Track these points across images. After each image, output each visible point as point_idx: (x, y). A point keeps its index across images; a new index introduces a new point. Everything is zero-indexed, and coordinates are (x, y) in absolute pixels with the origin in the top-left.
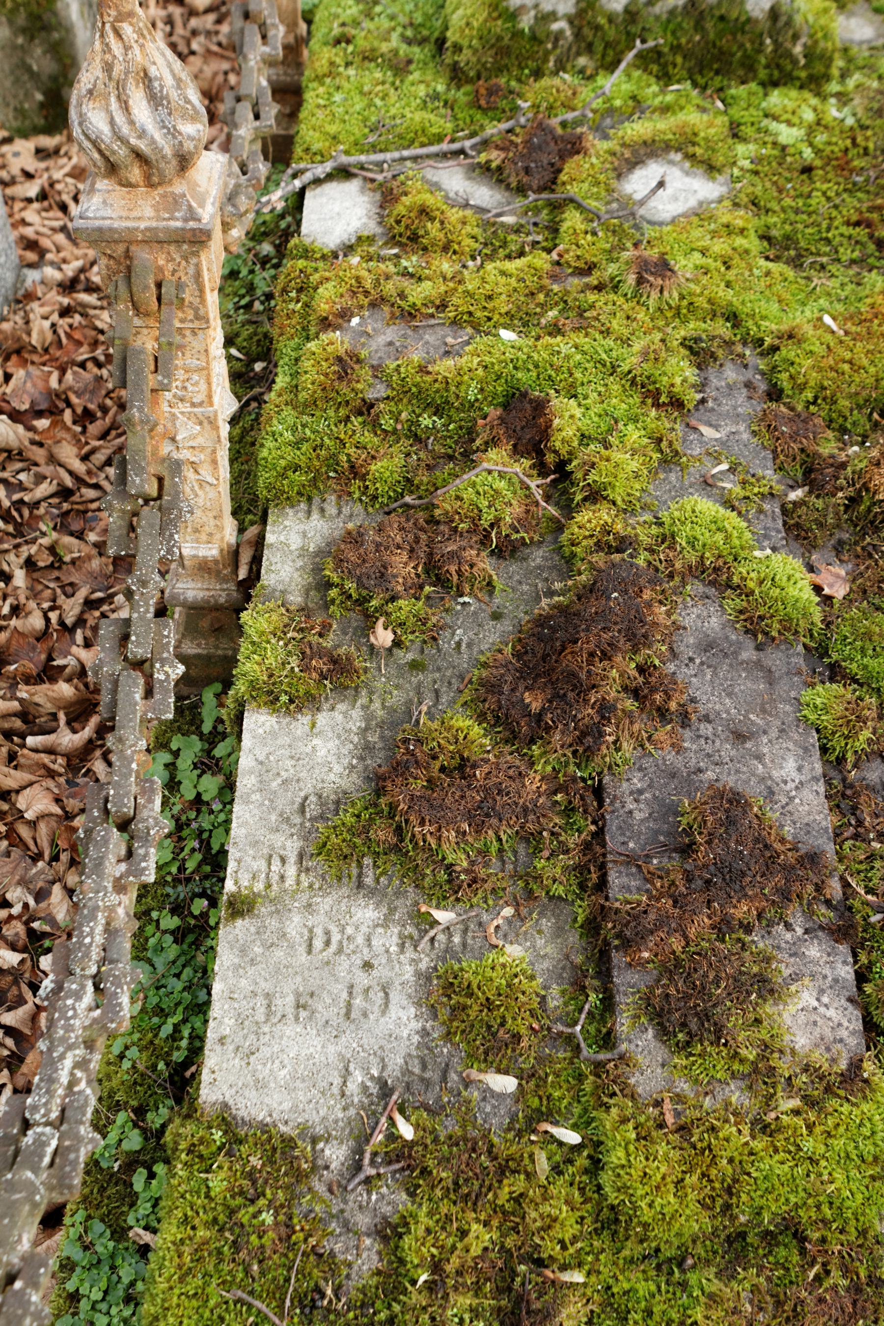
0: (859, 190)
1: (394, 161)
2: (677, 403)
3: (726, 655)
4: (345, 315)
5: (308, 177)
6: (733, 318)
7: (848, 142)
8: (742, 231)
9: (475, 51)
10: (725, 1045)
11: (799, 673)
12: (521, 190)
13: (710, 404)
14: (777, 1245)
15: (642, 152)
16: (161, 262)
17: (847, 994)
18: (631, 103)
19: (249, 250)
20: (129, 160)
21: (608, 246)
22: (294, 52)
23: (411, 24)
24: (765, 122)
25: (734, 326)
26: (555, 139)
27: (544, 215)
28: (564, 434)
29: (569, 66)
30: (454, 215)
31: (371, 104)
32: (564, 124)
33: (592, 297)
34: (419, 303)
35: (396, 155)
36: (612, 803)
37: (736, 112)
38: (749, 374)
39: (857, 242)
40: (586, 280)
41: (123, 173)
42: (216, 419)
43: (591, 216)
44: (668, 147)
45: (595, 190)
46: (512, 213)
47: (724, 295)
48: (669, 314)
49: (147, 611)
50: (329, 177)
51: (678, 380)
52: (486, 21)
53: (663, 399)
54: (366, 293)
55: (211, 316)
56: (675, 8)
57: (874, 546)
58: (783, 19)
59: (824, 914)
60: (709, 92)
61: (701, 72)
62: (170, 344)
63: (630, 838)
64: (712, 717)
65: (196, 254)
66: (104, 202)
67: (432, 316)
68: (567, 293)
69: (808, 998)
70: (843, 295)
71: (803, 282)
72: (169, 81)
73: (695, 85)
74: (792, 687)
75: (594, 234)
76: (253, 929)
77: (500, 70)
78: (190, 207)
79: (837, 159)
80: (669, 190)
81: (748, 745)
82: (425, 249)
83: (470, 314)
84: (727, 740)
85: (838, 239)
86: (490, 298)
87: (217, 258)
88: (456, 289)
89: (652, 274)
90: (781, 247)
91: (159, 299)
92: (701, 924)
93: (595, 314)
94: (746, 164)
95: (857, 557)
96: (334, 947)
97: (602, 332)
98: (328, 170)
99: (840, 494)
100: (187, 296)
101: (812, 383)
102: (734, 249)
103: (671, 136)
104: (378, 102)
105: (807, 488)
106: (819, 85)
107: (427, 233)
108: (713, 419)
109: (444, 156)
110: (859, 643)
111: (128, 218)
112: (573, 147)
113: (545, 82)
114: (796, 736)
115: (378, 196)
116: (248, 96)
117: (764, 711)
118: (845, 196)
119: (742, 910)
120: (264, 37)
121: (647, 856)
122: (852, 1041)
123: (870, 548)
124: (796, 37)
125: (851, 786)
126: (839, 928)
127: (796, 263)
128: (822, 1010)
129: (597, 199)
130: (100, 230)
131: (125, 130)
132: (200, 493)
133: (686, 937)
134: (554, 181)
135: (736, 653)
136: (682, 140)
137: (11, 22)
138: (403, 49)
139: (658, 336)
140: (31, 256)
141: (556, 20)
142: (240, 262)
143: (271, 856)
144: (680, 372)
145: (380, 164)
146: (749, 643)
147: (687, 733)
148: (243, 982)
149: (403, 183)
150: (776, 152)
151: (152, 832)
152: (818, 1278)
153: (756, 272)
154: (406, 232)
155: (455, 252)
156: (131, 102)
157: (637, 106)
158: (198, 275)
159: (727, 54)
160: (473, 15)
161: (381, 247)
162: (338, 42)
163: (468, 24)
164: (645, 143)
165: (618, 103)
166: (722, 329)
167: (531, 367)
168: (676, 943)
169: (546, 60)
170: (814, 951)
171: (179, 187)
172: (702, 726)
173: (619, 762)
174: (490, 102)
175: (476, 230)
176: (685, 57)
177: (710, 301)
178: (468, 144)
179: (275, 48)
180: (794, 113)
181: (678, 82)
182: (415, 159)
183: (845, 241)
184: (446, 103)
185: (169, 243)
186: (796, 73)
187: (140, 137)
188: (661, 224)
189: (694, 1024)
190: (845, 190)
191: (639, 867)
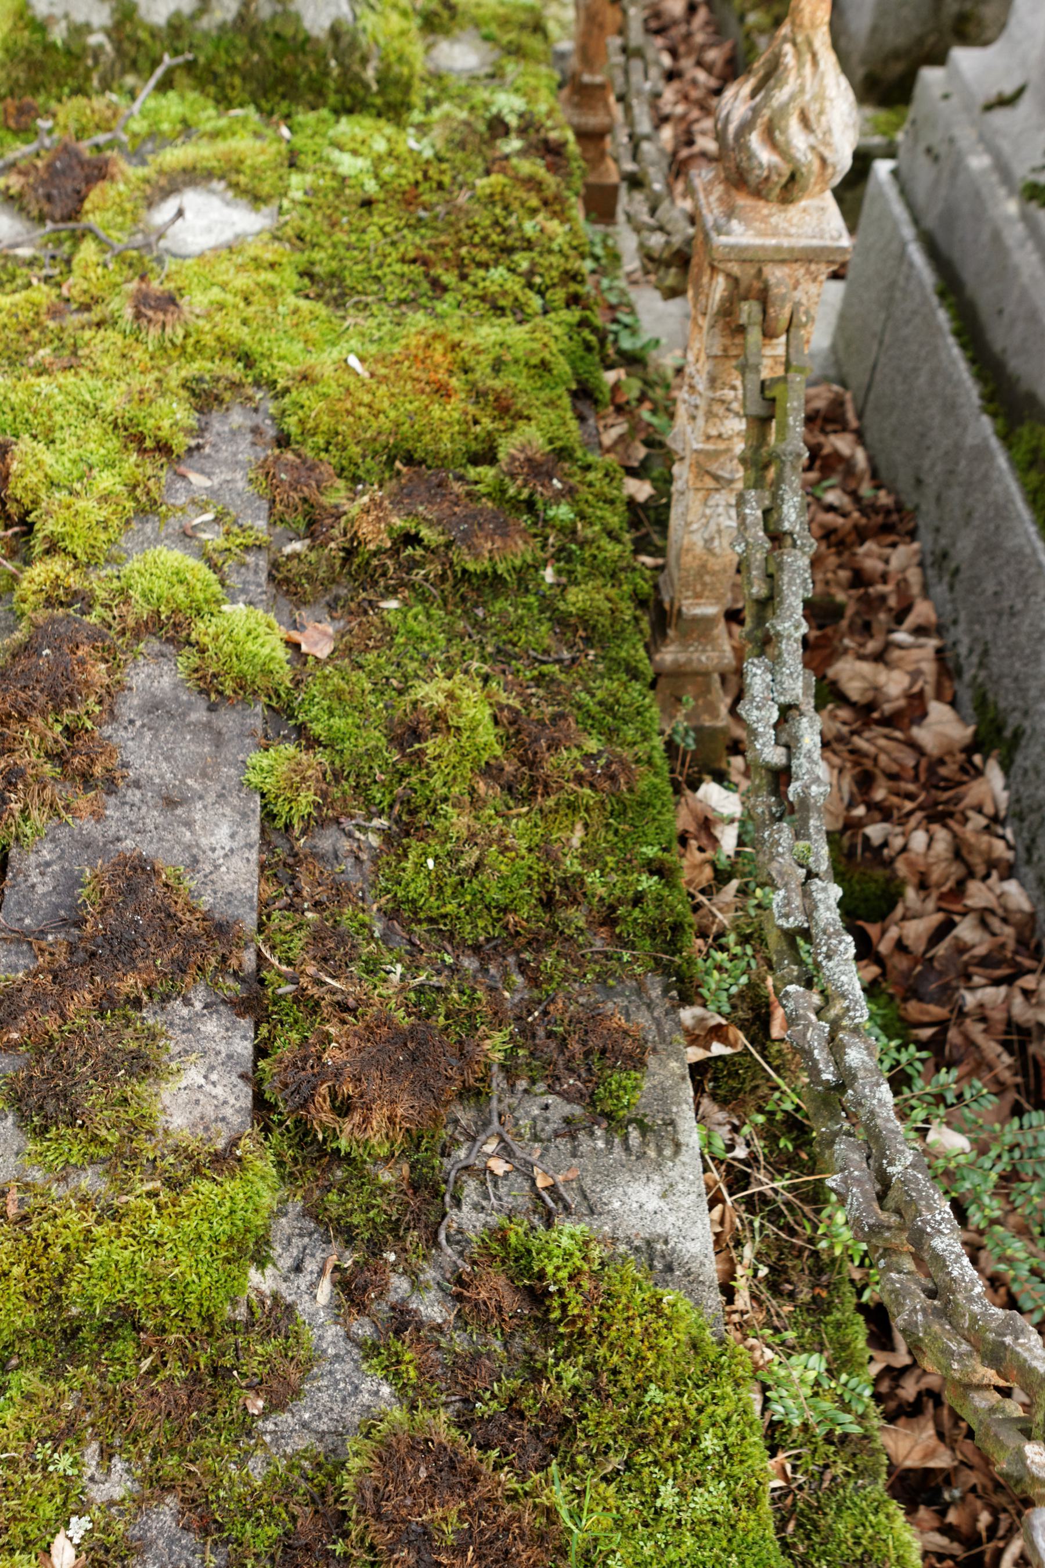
0: (426, 226)
2: (164, 448)
3: (172, 717)
6: (248, 360)
7: (419, 176)
8: (272, 266)
10: (81, 1127)
11: (253, 735)
13: (207, 450)
14: (117, 1337)
15: (180, 179)
17: (240, 1070)
25: (246, 366)
26: (82, 163)
28: (26, 480)
29: (115, 86)
32: (98, 147)
33: (88, 334)
36: (15, 877)
37: (299, 141)
38: (258, 419)
39: (410, 281)
44: (209, 175)
45: (120, 219)
46: (30, 243)
47: (237, 332)
51: (166, 423)
53: (149, 444)
56: (224, 23)
57: (370, 602)
58: (345, 40)
59: (231, 987)
60: (276, 117)
61: (265, 95)
64: (143, 782)
68: (62, 330)
69: (194, 1076)
70: (377, 335)
73: (259, 109)
74: (241, 751)
77: (36, 88)
79: (404, 193)
81: (179, 811)
84: (155, 807)
85: (389, 277)
89: (151, 308)
90: (328, 287)
92: (80, 1001)
94: (299, 195)
95: (351, 613)
97: (91, 372)
99: (332, 545)
101: (323, 428)
102: (258, 284)
103: (215, 164)
105: (308, 541)
106: (398, 115)
108: (208, 466)
110: (325, 703)
112: (99, 172)
114: (235, 801)
117: (204, 775)
118: (405, 232)
119: (130, 983)
121: (42, 932)
122: (236, 1120)
123: (365, 604)
124: (364, 60)
125: (296, 855)
126: (243, 1001)
127: (338, 302)
128: (208, 1088)
129: (121, 229)
133: (63, 1016)
134: (78, 212)
135: (184, 714)
136: (226, 167)
144: (172, 415)
146: (202, 704)
147: (112, 800)
150: (335, 184)
152: (153, 1371)
153: (281, 309)
157: (187, 129)
159: (283, 73)
166: (234, 371)
168: (51, 1023)
169: (88, 78)
170: (211, 1027)
173: (29, 832)
176: (244, 79)
177: (219, 339)
180: (363, 142)
181: (241, 105)
183: (396, 280)
186: (370, 100)
188: (184, 257)
189: (50, 1106)
191: (30, 943)
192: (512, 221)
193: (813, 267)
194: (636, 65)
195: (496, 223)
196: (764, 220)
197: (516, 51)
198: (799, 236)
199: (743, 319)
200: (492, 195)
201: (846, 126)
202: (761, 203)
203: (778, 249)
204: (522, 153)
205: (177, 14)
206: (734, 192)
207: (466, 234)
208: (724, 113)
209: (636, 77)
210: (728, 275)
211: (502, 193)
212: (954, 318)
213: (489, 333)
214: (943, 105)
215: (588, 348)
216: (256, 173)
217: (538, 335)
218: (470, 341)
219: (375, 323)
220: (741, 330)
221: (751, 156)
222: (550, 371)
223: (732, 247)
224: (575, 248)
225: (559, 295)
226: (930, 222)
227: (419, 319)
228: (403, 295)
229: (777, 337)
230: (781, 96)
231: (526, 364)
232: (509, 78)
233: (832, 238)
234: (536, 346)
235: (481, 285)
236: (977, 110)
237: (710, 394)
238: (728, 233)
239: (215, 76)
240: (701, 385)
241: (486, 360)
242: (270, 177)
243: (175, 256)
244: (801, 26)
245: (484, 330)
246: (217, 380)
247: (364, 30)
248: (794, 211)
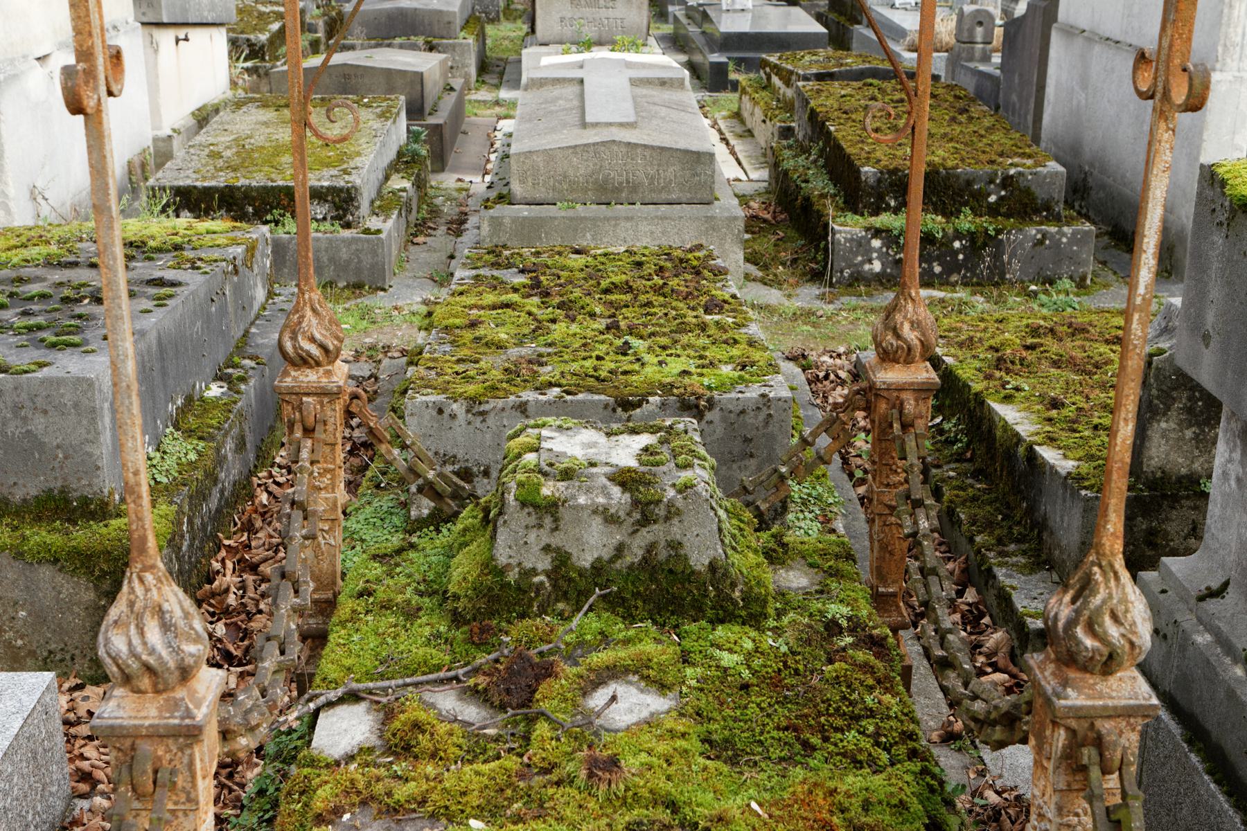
1: (398, 686)
4: (337, 811)
5: (322, 700)
6: (673, 806)
8: (683, 735)
9: (471, 599)
12: (503, 708)
15: (605, 675)
16: (160, 753)
18: (599, 637)
19: (279, 771)
20: (140, 672)
21: (569, 750)
22: (327, 607)
23: (424, 580)
24: (711, 650)
25: (673, 812)
26: (532, 666)
27: (522, 727)
29: (549, 610)
30: (442, 728)
31: (384, 642)
32: (541, 654)
33: (551, 791)
34: (402, 800)
35: (400, 682)
37: (687, 644)
40: (548, 777)
41: (134, 682)
43: (555, 724)
44: (627, 670)
46: (494, 725)
47: (664, 786)
48: (617, 804)
50: (341, 701)
52: (479, 576)
54: (359, 793)
55: (201, 799)
62: (159, 819)
65: (190, 746)
66: (118, 706)
67: (414, 811)
68: (530, 788)
70: (769, 785)
71: (736, 776)
72: (178, 613)
73: (655, 622)
75: (558, 739)
77: (492, 614)
79: (771, 678)
80: (620, 705)
82: (416, 757)
83: (447, 808)
86: (464, 794)
87: (210, 751)
88: (435, 788)
89: (601, 769)
90: (716, 747)
91: (155, 782)
93: (552, 804)
94: (693, 683)
97: (557, 819)
98: (340, 694)
100: (180, 781)
104: (390, 641)
106: (758, 622)
107: (418, 743)
109: (441, 682)
111: (136, 718)
112: (547, 671)
113: (527, 622)
115: (381, 715)
116: (276, 636)
120: (296, 592)
124: (733, 585)
127: (733, 761)
129: (564, 713)
130: (112, 727)
131: (139, 649)
137: (96, 587)
138: (416, 599)
139: (605, 820)
140: (84, 787)
141: (537, 575)
142: (268, 781)
145: (385, 689)
149: (403, 704)
154: (401, 743)
155: (441, 759)
156: (146, 629)
157: (605, 639)
158: (191, 764)
160: (469, 572)
161: (378, 757)
162: (360, 595)
163: (465, 579)
164: (607, 667)
165: (589, 637)
171: (180, 693)
174: (482, 639)
175: (461, 740)
177: (651, 791)
178: (461, 671)
179: (305, 600)
180: (735, 643)
182: (416, 685)
184: (447, 640)
185: (168, 736)
187: (150, 654)
190: (777, 702)
192: (855, 696)
193: (1132, 720)
194: (933, 579)
195: (844, 698)
196: (1092, 687)
197: (836, 574)
198: (1119, 698)
199: (1085, 761)
200: (837, 677)
201: (1144, 619)
202: (1088, 676)
203: (1105, 707)
204: (854, 646)
205: (599, 559)
206: (1064, 669)
207: (822, 707)
208: (1052, 614)
209: (935, 589)
210: (1068, 729)
211: (845, 676)
212: (1203, 761)
213: (853, 781)
214: (1162, 596)
215: (932, 790)
216: (662, 668)
217: (894, 781)
218: (843, 788)
219: (766, 775)
220: (1084, 769)
221: (1079, 643)
222: (907, 809)
223: (1070, 708)
224: (906, 715)
225: (902, 750)
226: (1167, 685)
227: (798, 773)
228: (783, 754)
229: (1112, 773)
230: (1097, 600)
231: (888, 804)
232: (834, 593)
233: (1144, 699)
234: (893, 789)
235: (840, 745)
236: (1193, 601)
237: (1058, 820)
238: (1066, 698)
239: (624, 600)
240: (1050, 813)
241: (856, 803)
242: (672, 671)
243: (607, 730)
244: (1104, 555)
245: (850, 779)
246: (653, 823)
247: (733, 564)
248: (1113, 681)
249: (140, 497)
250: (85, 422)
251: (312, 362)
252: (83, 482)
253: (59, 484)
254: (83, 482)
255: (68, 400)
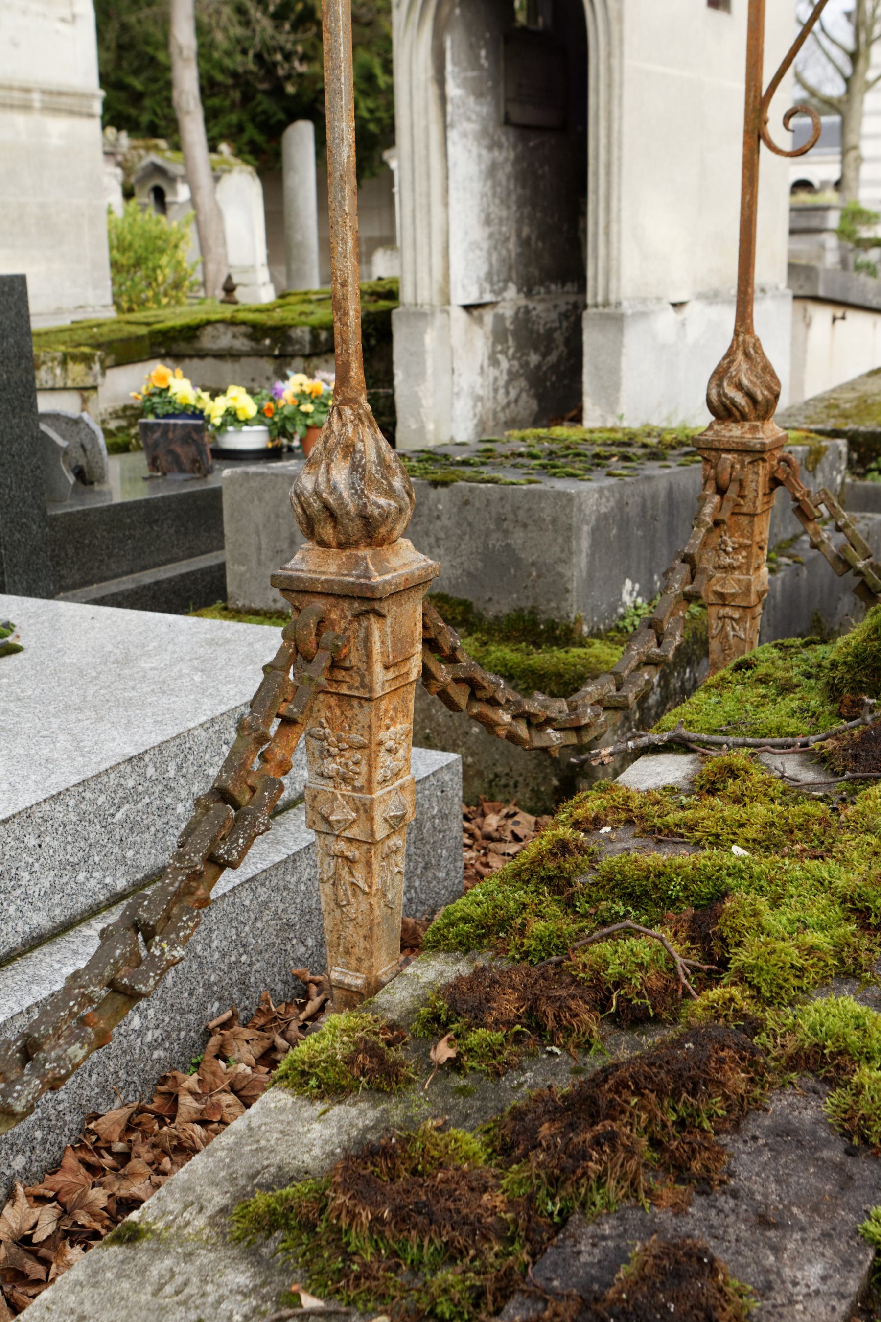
16: (333, 616)
35: (740, 740)
42: (371, 808)
49: (172, 884)
52: (864, 641)
63: (558, 1276)
76: (121, 1257)
78: (367, 567)
81: (771, 1234)
84: (746, 1221)
96: (182, 1297)
111: (315, 572)
130: (290, 578)
132: (353, 901)
143: (192, 1203)
148: (73, 1298)
151: (47, 1066)
158: (367, 641)
167: (747, 877)
172: (723, 1198)
187: (331, 493)
249: (346, 314)
250: (560, 540)
251: (737, 414)
252: (553, 605)
253: (530, 604)
254: (553, 605)
255: (547, 515)
